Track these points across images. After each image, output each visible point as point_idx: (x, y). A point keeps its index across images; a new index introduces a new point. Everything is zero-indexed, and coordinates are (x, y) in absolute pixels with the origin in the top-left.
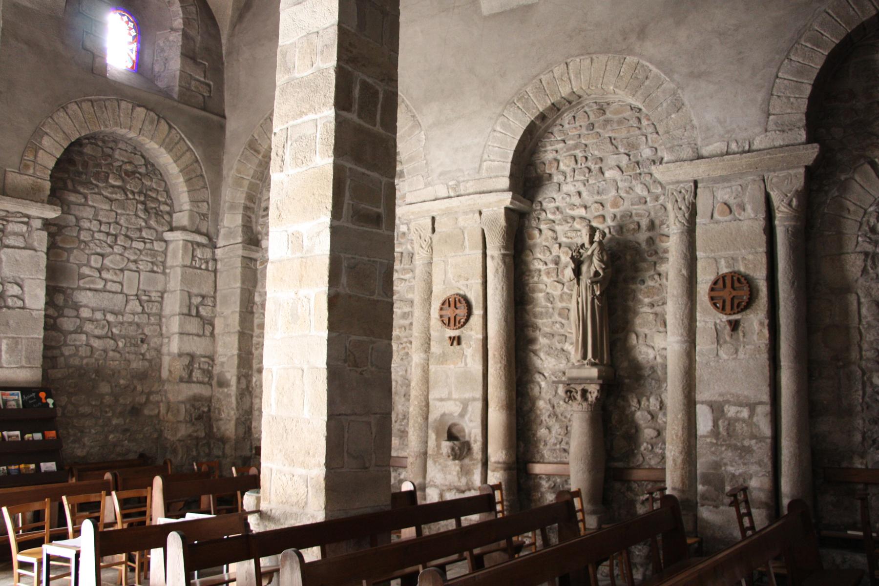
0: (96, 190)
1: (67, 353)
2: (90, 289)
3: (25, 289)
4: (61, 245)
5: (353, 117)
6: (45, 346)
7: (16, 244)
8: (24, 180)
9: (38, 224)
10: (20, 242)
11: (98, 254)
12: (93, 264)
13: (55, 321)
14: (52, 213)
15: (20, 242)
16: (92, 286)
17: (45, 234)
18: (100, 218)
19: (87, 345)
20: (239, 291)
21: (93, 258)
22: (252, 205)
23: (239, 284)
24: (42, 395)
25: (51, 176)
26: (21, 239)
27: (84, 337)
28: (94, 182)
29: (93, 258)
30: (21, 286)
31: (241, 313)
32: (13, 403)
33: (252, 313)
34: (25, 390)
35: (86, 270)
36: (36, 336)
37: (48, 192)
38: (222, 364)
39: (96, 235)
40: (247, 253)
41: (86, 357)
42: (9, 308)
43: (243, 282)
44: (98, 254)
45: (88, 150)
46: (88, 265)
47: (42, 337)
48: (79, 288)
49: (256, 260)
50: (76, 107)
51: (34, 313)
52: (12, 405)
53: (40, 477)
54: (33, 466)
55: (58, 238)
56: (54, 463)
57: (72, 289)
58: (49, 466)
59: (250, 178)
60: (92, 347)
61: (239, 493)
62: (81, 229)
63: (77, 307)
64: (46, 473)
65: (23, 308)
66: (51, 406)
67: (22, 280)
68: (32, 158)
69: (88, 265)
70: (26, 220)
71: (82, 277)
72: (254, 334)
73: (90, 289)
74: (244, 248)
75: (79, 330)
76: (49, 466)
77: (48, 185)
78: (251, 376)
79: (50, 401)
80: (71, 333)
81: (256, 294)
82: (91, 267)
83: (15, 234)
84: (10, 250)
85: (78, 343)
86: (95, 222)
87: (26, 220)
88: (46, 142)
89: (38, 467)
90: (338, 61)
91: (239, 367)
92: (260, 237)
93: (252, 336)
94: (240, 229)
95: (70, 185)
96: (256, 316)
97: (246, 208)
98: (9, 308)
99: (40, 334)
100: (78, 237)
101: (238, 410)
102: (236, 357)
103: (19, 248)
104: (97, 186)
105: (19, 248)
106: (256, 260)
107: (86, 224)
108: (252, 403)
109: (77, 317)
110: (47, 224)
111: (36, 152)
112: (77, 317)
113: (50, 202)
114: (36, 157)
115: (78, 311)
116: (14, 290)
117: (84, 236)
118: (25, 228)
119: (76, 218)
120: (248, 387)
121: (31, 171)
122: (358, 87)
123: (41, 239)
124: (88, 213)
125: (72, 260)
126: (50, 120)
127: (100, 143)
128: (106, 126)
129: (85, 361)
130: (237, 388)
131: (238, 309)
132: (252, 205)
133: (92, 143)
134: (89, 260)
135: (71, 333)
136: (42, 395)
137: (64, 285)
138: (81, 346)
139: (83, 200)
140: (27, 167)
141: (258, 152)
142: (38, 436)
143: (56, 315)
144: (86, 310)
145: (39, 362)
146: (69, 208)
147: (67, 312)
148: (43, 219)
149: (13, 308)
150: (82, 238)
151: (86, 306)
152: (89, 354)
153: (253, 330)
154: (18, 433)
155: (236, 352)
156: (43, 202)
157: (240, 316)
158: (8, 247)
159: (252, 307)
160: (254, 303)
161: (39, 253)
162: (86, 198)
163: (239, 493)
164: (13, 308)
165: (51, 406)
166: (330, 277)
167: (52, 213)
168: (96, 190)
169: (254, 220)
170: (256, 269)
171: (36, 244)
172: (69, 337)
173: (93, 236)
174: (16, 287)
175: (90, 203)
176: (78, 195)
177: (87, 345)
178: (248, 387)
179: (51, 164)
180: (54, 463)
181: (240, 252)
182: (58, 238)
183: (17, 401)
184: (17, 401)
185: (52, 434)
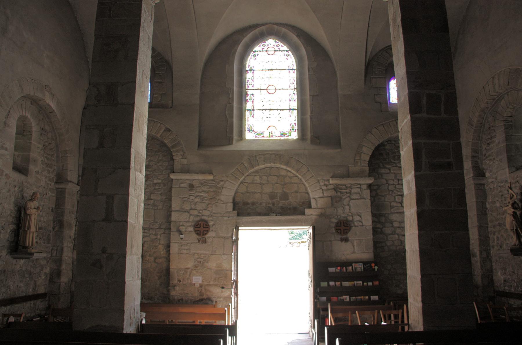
0: (394, 165)
1: (389, 245)
2: (397, 213)
3: (362, 217)
4: (380, 194)
5: (424, 115)
6: (374, 242)
7: (357, 198)
8: (357, 169)
9: (365, 187)
10: (358, 196)
11: (400, 195)
12: (397, 200)
13: (382, 230)
14: (370, 181)
15: (358, 196)
16: (398, 211)
17: (369, 191)
18: (398, 178)
19: (398, 240)
20: (475, 203)
21: (397, 197)
22: (477, 155)
23: (475, 200)
24: (373, 265)
25: (368, 164)
26: (358, 195)
27: (396, 236)
28: (393, 161)
29: (397, 197)
30: (360, 216)
31: (478, 215)
32: (359, 269)
33: (486, 214)
34: (364, 263)
35: (394, 204)
36: (369, 238)
37: (368, 172)
38: (473, 244)
39: (397, 186)
40: (477, 182)
41: (399, 245)
42: (356, 226)
43: (477, 198)
44: (400, 195)
45: (388, 147)
46: (395, 201)
47: (372, 238)
48: (392, 213)
49: (484, 185)
50: (375, 130)
51: (367, 227)
52: (359, 270)
53: (370, 302)
54: (367, 297)
55: (378, 191)
56: (377, 297)
57: (388, 214)
58: (375, 298)
59: (471, 140)
60: (401, 240)
61: (333, 324)
62: (389, 185)
63: (391, 222)
64: (373, 301)
65: (362, 226)
66: (376, 270)
67: (361, 213)
68: (359, 158)
69: (395, 201)
70: (359, 186)
71: (392, 207)
72: (489, 226)
73: (397, 213)
74: (474, 179)
75: (394, 233)
76: (375, 298)
77: (367, 168)
78: (490, 250)
79: (376, 268)
80: (390, 234)
81: (487, 203)
82: (397, 202)
83: (356, 193)
84: (354, 201)
85: (393, 239)
86: (395, 180)
87: (359, 186)
88: (364, 149)
89: (370, 298)
90: (408, 90)
91: (480, 245)
92: (484, 171)
93: (488, 227)
94: (471, 169)
95: (381, 165)
96: (488, 215)
97: (473, 157)
98: (356, 226)
99: (371, 237)
100: (388, 189)
101: (482, 270)
102: (478, 240)
103: (358, 199)
104: (394, 163)
105: (358, 199)
106: (484, 185)
107: (391, 182)
108: (492, 265)
109: (392, 227)
110: (370, 186)
111: (360, 155)
112: (392, 227)
113: (370, 175)
114: (360, 157)
115: (392, 224)
116: (357, 218)
117: (391, 188)
118: (359, 190)
119: (387, 180)
120: (488, 256)
121: (359, 164)
122: (425, 98)
123: (367, 193)
124: (392, 176)
125: (386, 200)
126: (365, 139)
127: (393, 142)
128: (391, 134)
129: (398, 248)
130: (480, 257)
131: (476, 213)
132: (477, 155)
133: (389, 143)
134: (395, 199)
135: (390, 234)
136: (373, 265)
137: (384, 212)
138: (396, 240)
139: (388, 171)
140: (357, 162)
141: (472, 125)
142: (370, 284)
143: (381, 227)
144: (396, 223)
145: (372, 250)
146: (382, 176)
147: (387, 225)
148: (367, 184)
149: (358, 226)
150: (390, 189)
151: (395, 221)
152: (400, 244)
153: (488, 224)
154: (361, 282)
155: (477, 237)
156: (365, 177)
157: (477, 217)
158: (353, 199)
159: (486, 211)
160: (486, 209)
161: (367, 200)
162: (390, 170)
163: (333, 324)
164: (358, 226)
165: (376, 270)
166: (465, 198)
167: (370, 181)
168: (394, 165)
169: (479, 162)
170: (486, 190)
171: (365, 196)
172: (389, 237)
173: (395, 187)
174: (358, 217)
175: (392, 171)
176: (385, 169)
177: (398, 240)
178: (488, 256)
179: (368, 158)
180: (377, 297)
181: (472, 182)
182: (378, 191)
183: (361, 268)
184: (361, 268)
185: (377, 283)
